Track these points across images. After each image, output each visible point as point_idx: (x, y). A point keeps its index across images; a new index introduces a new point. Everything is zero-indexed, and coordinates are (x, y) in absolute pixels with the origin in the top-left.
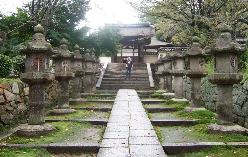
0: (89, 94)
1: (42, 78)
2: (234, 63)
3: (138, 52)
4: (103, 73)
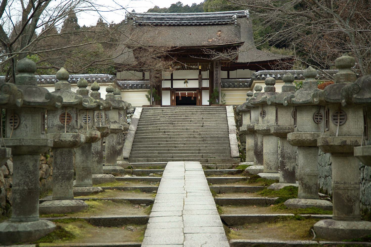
0: (114, 168)
1: (72, 139)
2: (318, 119)
3: (208, 78)
4: (133, 128)
